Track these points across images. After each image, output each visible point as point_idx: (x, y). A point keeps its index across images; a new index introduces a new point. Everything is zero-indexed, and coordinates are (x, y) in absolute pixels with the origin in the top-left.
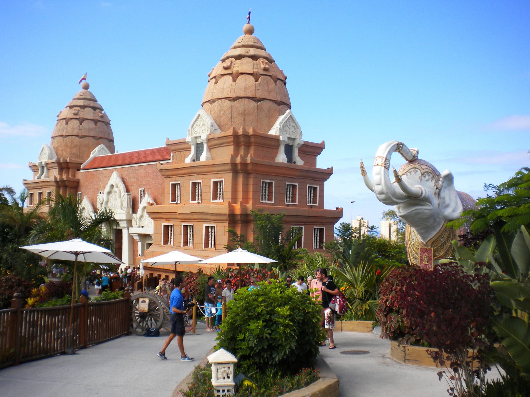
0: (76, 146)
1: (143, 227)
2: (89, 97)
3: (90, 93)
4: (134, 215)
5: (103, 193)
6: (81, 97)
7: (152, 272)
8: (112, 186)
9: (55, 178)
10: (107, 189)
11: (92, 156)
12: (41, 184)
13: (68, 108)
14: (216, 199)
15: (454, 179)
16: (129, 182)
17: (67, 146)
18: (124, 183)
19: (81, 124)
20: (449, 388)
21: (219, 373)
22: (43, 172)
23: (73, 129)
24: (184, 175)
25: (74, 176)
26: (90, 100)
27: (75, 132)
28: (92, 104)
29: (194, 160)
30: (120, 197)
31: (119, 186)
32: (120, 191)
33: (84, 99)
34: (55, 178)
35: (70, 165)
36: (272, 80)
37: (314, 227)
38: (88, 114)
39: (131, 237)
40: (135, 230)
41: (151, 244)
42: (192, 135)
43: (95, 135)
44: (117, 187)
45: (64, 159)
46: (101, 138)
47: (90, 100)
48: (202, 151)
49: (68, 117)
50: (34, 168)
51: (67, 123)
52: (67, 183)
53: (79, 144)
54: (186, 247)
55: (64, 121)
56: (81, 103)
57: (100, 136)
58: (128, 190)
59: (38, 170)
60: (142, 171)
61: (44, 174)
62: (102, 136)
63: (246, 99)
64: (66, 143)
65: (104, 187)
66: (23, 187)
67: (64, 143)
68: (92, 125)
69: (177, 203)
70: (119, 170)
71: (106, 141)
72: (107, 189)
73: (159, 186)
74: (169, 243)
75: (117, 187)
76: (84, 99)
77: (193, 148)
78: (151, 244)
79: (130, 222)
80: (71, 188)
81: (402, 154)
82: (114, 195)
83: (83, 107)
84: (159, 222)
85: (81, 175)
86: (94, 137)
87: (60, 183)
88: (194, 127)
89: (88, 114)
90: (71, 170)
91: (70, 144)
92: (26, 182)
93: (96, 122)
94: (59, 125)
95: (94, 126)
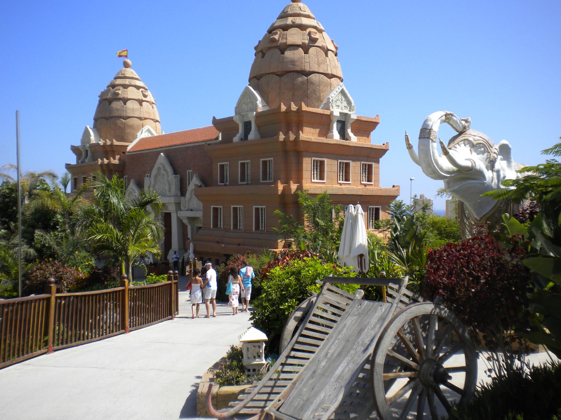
4: (183, 198)
5: (150, 176)
10: (154, 172)
14: (266, 179)
15: (512, 151)
20: (487, 369)
21: (249, 353)
29: (242, 139)
36: (322, 52)
37: (370, 207)
39: (180, 220)
40: (184, 214)
48: (250, 129)
61: (88, 158)
63: (295, 73)
65: (151, 170)
66: (65, 171)
69: (225, 185)
81: (452, 125)
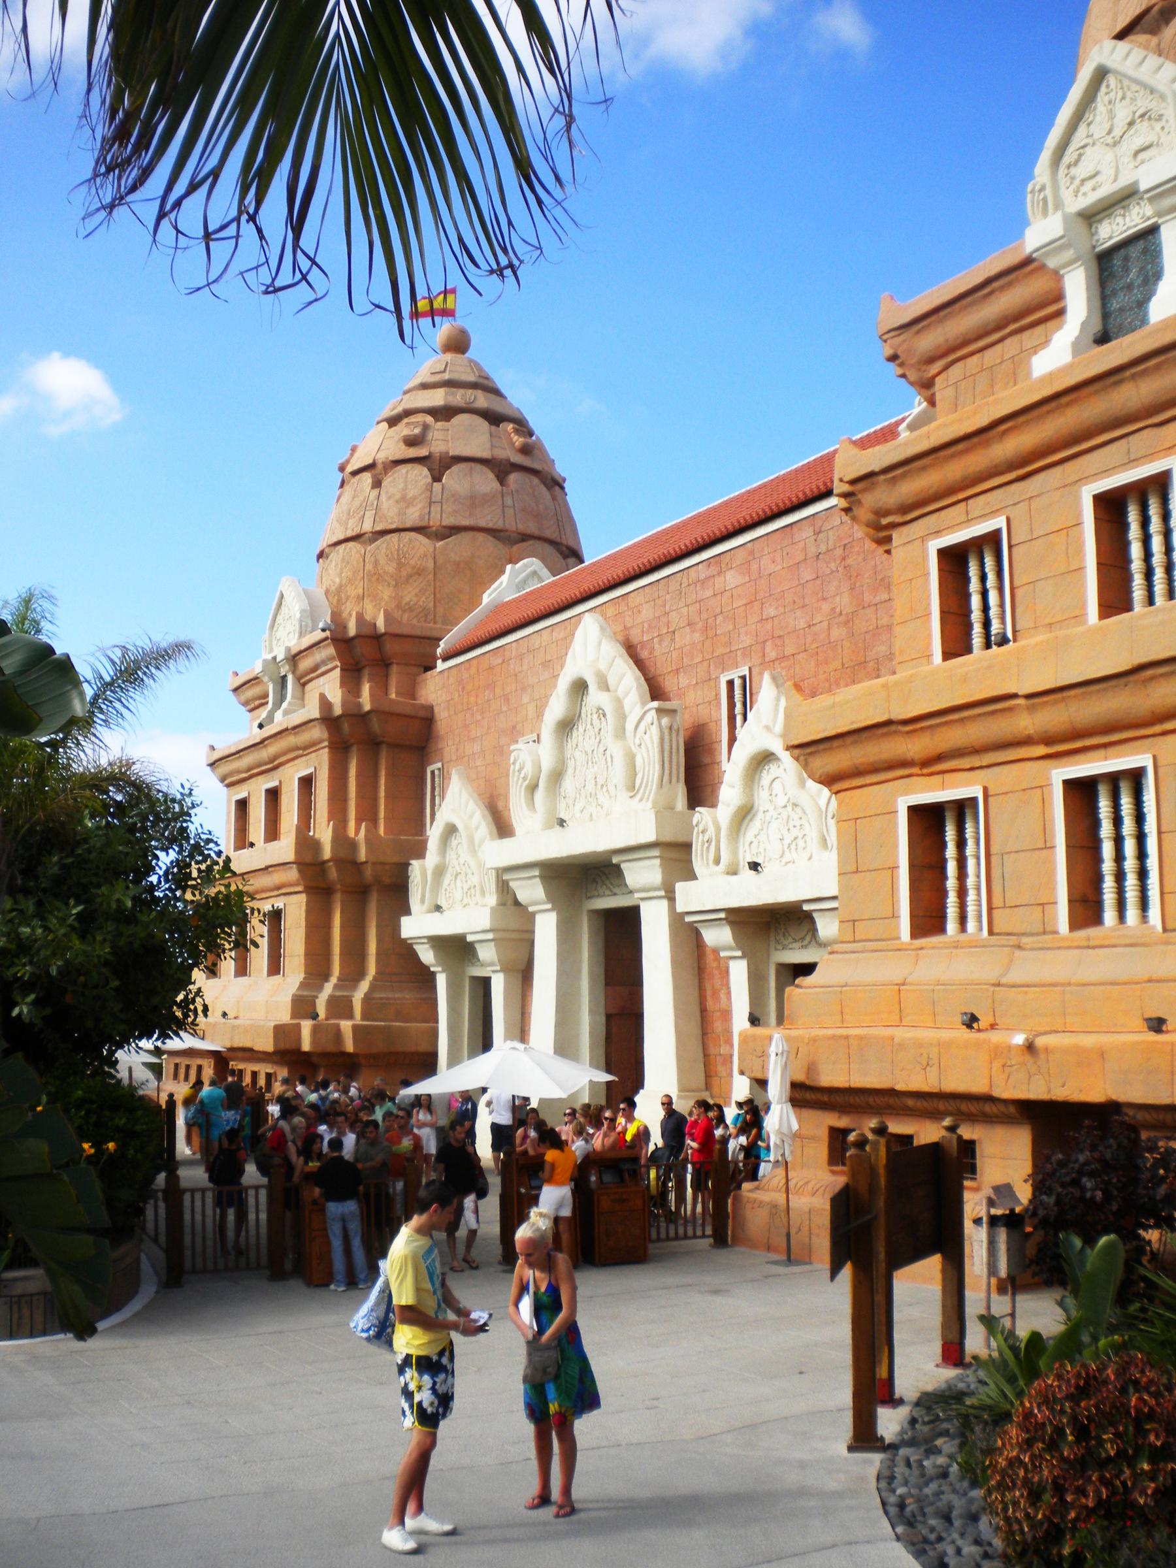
0: (420, 572)
1: (754, 866)
2: (471, 378)
3: (473, 364)
6: (437, 378)
7: (842, 1122)
8: (580, 687)
9: (325, 704)
11: (486, 598)
12: (272, 749)
13: (385, 425)
16: (661, 655)
17: (376, 577)
18: (639, 663)
19: (437, 478)
22: (281, 698)
23: (405, 501)
24: (1025, 466)
25: (411, 691)
26: (474, 386)
27: (413, 516)
28: (482, 400)
30: (620, 733)
31: (612, 681)
32: (619, 703)
33: (450, 384)
34: (325, 704)
35: (390, 647)
38: (468, 437)
39: (687, 934)
40: (713, 889)
41: (807, 969)
42: (1058, 205)
43: (499, 525)
44: (605, 686)
45: (360, 618)
46: (525, 537)
47: (474, 386)
49: (381, 457)
50: (250, 693)
51: (377, 484)
52: (376, 726)
53: (431, 564)
54: (1092, 932)
55: (367, 478)
56: (437, 398)
57: (521, 527)
58: (656, 692)
59: (266, 696)
60: (732, 579)
61: (285, 705)
62: (532, 528)
64: (376, 563)
67: (369, 567)
68: (486, 481)
70: (611, 611)
71: (549, 550)
72: (557, 707)
73: (837, 632)
74: (952, 926)
75: (605, 686)
76: (450, 384)
77: (1077, 291)
78: (807, 969)
79: (678, 856)
80: (395, 746)
82: (591, 732)
83: (444, 413)
84: (871, 796)
85: (436, 689)
86: (493, 532)
87: (346, 727)
88: (1070, 155)
89: (468, 437)
90: (394, 669)
91: (391, 568)
92: (217, 755)
93: (501, 469)
94: (346, 498)
95: (495, 485)
